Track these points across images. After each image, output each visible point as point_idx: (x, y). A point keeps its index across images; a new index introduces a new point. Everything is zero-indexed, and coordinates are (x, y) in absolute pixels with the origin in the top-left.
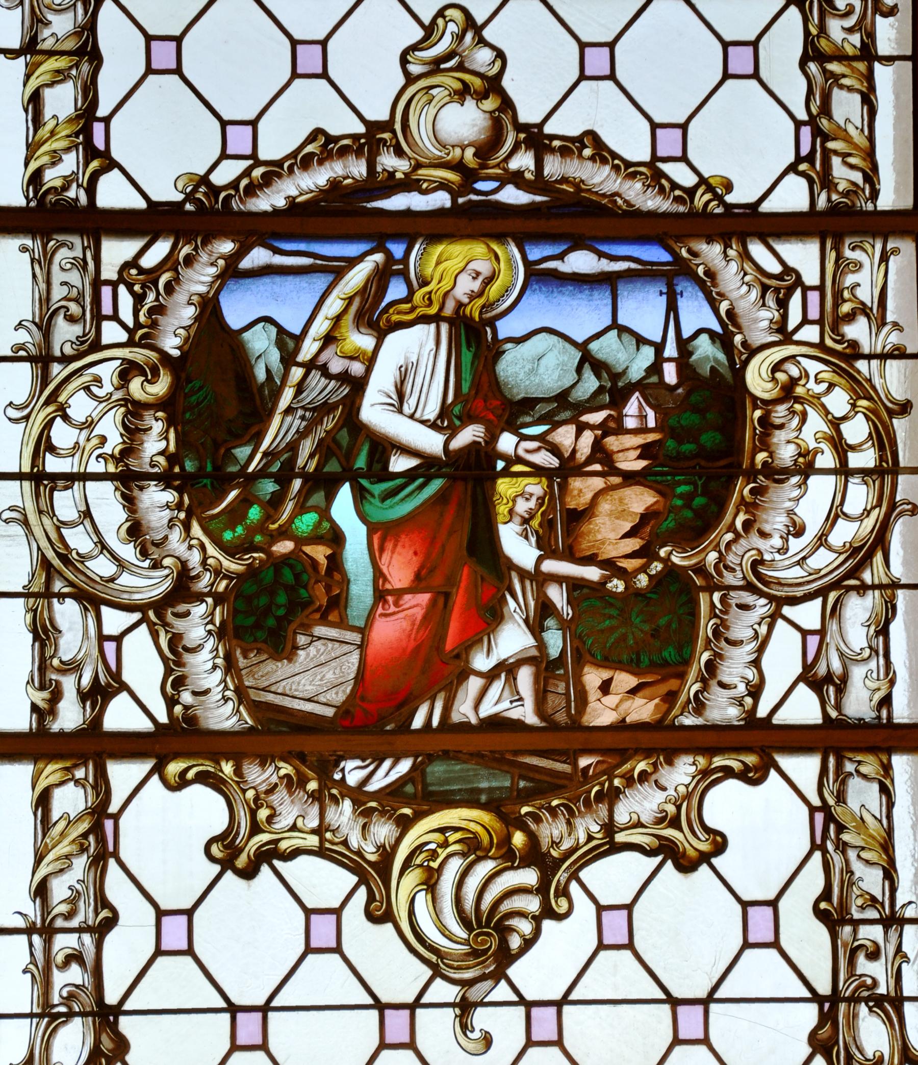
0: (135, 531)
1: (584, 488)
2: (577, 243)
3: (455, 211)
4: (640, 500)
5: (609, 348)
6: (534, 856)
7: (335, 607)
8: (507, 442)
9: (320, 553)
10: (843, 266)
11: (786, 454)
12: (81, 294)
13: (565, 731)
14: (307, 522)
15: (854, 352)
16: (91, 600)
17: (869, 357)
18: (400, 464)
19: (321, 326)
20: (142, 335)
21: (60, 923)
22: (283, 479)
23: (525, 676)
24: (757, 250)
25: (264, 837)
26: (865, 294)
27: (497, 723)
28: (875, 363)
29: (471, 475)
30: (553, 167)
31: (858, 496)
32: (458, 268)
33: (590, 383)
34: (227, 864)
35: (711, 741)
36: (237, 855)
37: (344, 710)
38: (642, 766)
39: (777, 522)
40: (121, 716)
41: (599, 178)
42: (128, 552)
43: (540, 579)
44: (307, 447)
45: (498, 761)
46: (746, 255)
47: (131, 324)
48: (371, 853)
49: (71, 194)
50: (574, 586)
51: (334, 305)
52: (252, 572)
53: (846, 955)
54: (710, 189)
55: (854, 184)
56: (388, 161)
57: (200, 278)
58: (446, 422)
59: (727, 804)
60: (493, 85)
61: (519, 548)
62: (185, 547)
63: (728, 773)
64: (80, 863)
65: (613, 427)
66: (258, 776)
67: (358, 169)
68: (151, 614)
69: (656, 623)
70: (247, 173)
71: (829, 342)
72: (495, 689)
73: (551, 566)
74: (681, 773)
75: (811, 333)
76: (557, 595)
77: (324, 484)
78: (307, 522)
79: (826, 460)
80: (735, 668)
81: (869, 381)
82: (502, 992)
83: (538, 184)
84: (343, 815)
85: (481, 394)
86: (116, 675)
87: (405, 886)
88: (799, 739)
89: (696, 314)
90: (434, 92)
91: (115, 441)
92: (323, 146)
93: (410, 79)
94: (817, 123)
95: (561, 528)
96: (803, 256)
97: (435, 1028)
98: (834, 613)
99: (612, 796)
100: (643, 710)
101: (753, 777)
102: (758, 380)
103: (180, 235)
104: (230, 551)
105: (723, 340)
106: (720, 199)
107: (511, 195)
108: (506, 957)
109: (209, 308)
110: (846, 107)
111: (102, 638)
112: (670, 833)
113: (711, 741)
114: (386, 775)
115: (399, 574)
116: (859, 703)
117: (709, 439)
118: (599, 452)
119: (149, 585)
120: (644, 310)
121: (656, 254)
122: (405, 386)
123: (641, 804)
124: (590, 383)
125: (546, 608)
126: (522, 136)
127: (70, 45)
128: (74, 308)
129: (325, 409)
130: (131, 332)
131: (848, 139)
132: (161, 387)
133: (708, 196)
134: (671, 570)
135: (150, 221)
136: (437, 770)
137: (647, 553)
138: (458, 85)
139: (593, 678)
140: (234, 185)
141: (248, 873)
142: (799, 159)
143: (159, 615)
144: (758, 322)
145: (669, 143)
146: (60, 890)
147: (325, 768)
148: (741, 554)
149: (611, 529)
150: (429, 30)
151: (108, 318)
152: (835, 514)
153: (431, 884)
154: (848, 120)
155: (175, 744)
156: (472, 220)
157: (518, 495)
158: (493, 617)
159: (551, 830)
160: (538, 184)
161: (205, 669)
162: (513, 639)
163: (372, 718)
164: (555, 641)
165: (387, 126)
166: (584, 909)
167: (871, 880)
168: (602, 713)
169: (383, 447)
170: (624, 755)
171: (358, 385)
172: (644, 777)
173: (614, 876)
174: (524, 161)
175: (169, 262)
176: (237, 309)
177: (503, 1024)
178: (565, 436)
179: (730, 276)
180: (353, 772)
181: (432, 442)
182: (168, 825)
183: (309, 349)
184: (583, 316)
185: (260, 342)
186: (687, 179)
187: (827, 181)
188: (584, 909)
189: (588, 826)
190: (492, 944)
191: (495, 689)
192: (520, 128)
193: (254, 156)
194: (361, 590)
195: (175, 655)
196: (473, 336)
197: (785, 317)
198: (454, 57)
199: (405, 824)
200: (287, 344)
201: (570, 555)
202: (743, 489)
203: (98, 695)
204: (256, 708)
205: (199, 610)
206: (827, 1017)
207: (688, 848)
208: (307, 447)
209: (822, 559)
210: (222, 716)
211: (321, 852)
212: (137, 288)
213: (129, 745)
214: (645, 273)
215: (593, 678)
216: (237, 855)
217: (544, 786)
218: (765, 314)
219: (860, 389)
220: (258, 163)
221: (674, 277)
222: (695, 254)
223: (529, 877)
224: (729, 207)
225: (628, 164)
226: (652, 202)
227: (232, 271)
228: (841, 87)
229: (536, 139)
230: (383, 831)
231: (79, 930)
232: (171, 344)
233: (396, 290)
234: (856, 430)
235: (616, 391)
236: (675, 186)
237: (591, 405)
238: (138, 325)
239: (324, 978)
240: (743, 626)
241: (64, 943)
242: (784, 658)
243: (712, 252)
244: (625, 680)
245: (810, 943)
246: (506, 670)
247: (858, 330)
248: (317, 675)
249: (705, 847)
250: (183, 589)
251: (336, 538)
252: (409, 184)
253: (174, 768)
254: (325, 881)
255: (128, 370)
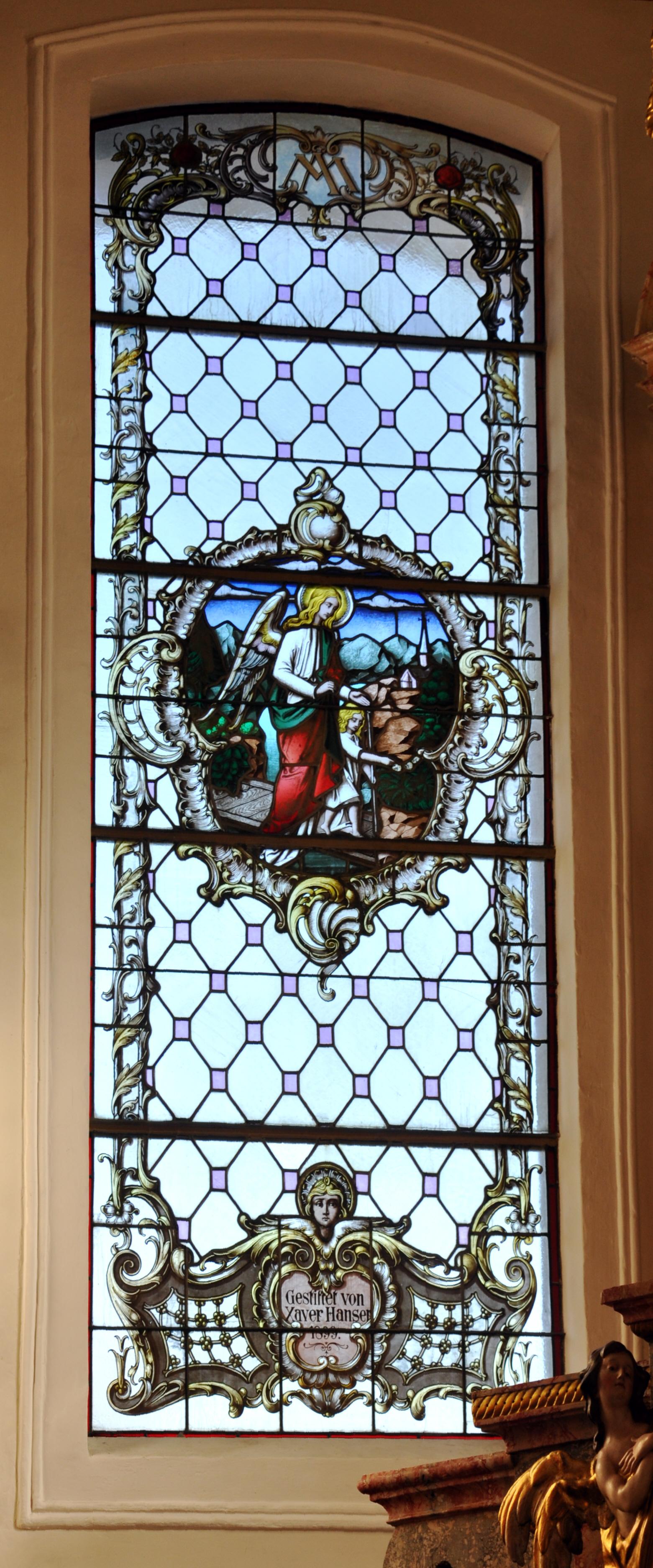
0: (164, 726)
1: (382, 717)
2: (379, 592)
3: (319, 572)
4: (409, 725)
5: (394, 646)
6: (357, 903)
7: (261, 772)
8: (345, 691)
9: (253, 743)
10: (506, 612)
11: (479, 705)
12: (138, 605)
13: (371, 840)
14: (247, 727)
15: (510, 655)
16: (142, 760)
17: (518, 658)
18: (293, 700)
19: (254, 627)
20: (168, 627)
21: (127, 924)
22: (236, 704)
23: (353, 812)
24: (465, 600)
25: (226, 886)
26: (517, 626)
27: (339, 835)
28: (520, 661)
29: (326, 708)
30: (367, 552)
31: (513, 729)
32: (321, 601)
33: (385, 664)
34: (208, 899)
35: (442, 849)
36: (212, 895)
37: (265, 824)
38: (409, 860)
39: (474, 740)
40: (156, 821)
41: (390, 559)
42: (160, 738)
43: (360, 763)
44: (247, 688)
45: (340, 854)
46: (459, 603)
47: (162, 621)
48: (278, 897)
49: (134, 554)
50: (377, 766)
51: (261, 617)
52: (220, 751)
53: (505, 960)
54: (442, 568)
55: (510, 570)
56: (287, 545)
57: (196, 600)
58: (316, 679)
59: (450, 882)
60: (338, 510)
61: (350, 746)
62: (189, 736)
63: (450, 866)
64: (137, 894)
65: (396, 687)
66: (224, 855)
67: (273, 548)
68: (171, 770)
69: (415, 788)
70: (219, 547)
71: (499, 650)
72: (340, 814)
73: (366, 756)
74: (428, 865)
75: (490, 645)
76: (369, 771)
77: (255, 709)
78: (247, 727)
79: (497, 709)
80: (454, 813)
81: (518, 670)
82: (340, 970)
83: (360, 560)
84: (264, 876)
85: (332, 666)
86: (154, 800)
87: (294, 915)
88: (484, 851)
89: (436, 632)
90: (310, 511)
91: (154, 681)
92: (256, 536)
93: (298, 504)
94: (493, 538)
95: (370, 737)
96: (487, 605)
97: (309, 986)
98: (501, 788)
99: (394, 875)
100: (409, 832)
101: (462, 868)
102: (465, 666)
103: (186, 577)
104: (210, 739)
105: (448, 645)
106: (447, 573)
107: (347, 565)
108: (343, 953)
109: (200, 614)
110: (507, 531)
111: (147, 781)
112: (422, 895)
113: (442, 849)
114: (288, 857)
115: (292, 757)
116: (512, 834)
117: (442, 695)
118: (389, 699)
119: (171, 755)
120: (411, 628)
121: (417, 600)
122: (295, 660)
123: (408, 880)
124: (385, 664)
125: (363, 778)
126: (352, 536)
127: (134, 479)
128: (134, 612)
129: (256, 670)
130: (162, 625)
131: (507, 547)
132: (176, 654)
133: (441, 572)
134: (423, 760)
135: (171, 569)
136: (310, 857)
137: (412, 752)
138: (321, 508)
139: (386, 814)
140: (213, 553)
141: (218, 904)
142: (484, 556)
143: (176, 770)
144: (466, 636)
145: (423, 543)
146: (127, 907)
147: (256, 853)
148: (457, 756)
149: (394, 740)
150: (308, 479)
151: (151, 618)
152: (502, 738)
153: (307, 913)
154: (507, 537)
155: (183, 836)
156: (327, 577)
157: (350, 718)
158: (338, 781)
159: (365, 891)
160: (360, 560)
161: (197, 797)
162: (347, 793)
163: (278, 829)
164: (367, 794)
165: (287, 527)
166: (380, 931)
167: (517, 923)
168: (390, 832)
169: (285, 690)
170: (401, 854)
171: (272, 658)
172: (410, 866)
173: (395, 915)
174: (353, 548)
175: (181, 591)
176: (214, 617)
177: (341, 986)
178: (373, 690)
179: (452, 612)
180: (269, 856)
181: (308, 689)
182: (180, 878)
183: (249, 638)
184: (382, 630)
185: (225, 633)
186: (432, 562)
187: (497, 567)
188: (380, 931)
189: (383, 889)
190: (335, 948)
191: (340, 814)
192: (351, 531)
193: (222, 539)
194: (274, 763)
195: (183, 791)
196: (328, 636)
197: (478, 635)
198: (319, 494)
199: (294, 884)
200: (239, 635)
201: (375, 751)
202: (458, 722)
203: (146, 809)
204: (223, 821)
205: (195, 769)
206: (495, 991)
207: (431, 904)
208: (247, 688)
209: (496, 760)
210: (207, 824)
211: (254, 895)
212: (165, 603)
213: (160, 836)
214: (411, 609)
215: (386, 814)
216: (212, 895)
217: (361, 868)
218: (469, 633)
219: (513, 674)
220: (224, 543)
221: (425, 612)
222: (435, 601)
223: (354, 913)
224: (451, 578)
225: (403, 553)
226: (415, 573)
227: (211, 598)
228: (504, 520)
229: (359, 537)
230: (284, 887)
231: (134, 400)
232: (182, 632)
233: (291, 611)
234: (512, 695)
235: (397, 668)
236: (425, 565)
237: (385, 675)
238: (166, 622)
239: (254, 959)
240: (458, 792)
241: (129, 934)
242: (477, 810)
243: (443, 600)
244: (401, 816)
245: (487, 953)
246: (344, 807)
247: (512, 644)
248: (252, 805)
249: (438, 903)
250: (187, 758)
251: (261, 736)
252: (298, 557)
253: (182, 849)
254: (255, 910)
255: (161, 645)
